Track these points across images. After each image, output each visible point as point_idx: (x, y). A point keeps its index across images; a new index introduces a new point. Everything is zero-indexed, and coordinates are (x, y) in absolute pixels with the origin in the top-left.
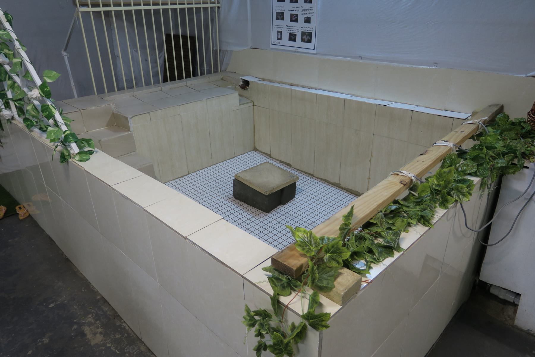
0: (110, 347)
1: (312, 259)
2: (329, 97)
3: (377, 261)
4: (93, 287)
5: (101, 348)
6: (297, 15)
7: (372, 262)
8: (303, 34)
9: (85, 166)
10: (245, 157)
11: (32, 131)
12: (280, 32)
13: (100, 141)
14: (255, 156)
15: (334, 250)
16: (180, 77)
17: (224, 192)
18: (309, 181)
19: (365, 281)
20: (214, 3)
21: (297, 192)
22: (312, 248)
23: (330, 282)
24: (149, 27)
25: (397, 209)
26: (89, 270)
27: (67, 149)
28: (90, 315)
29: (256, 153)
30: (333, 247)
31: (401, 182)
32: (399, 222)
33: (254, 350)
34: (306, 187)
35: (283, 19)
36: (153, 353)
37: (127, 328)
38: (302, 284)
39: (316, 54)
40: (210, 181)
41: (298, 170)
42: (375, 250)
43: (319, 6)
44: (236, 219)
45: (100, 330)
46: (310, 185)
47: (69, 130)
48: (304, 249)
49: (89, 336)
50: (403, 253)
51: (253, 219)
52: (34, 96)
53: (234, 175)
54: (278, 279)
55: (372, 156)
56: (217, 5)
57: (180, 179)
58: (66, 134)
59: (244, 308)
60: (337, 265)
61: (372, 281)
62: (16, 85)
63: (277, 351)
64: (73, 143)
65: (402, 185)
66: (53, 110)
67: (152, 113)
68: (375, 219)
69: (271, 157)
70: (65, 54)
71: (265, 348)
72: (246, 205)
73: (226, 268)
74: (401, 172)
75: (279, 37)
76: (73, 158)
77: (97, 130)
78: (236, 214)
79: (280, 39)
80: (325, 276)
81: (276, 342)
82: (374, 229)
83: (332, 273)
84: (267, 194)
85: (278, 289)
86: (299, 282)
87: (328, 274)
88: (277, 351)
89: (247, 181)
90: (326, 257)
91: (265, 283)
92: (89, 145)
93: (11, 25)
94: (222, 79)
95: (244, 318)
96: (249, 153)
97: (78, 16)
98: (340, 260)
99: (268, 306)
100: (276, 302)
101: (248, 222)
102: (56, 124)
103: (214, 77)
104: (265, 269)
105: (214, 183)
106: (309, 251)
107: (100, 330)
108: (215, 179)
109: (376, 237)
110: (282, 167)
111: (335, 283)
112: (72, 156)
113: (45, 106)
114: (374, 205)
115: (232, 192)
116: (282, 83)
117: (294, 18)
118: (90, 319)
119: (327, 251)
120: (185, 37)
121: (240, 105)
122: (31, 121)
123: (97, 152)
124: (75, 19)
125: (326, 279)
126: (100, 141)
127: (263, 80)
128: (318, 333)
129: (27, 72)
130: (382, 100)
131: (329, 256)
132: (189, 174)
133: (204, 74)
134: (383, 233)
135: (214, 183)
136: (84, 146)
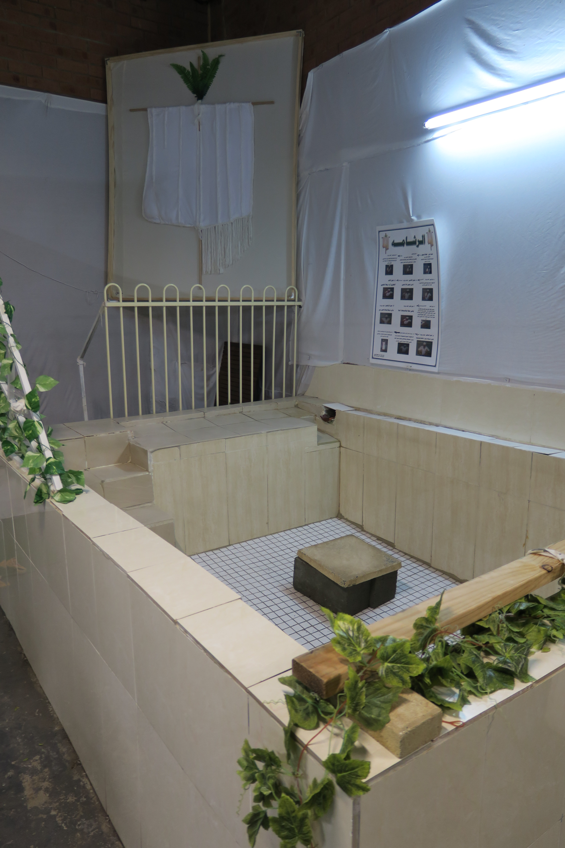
0: (55, 816)
1: (359, 669)
2: (456, 438)
3: (480, 692)
4: (53, 710)
5: (40, 816)
6: (411, 317)
7: (470, 693)
8: (419, 343)
9: (66, 509)
10: (322, 527)
11: (10, 459)
12: (385, 341)
13: (103, 482)
14: (338, 527)
15: (398, 656)
16: (235, 401)
17: (279, 578)
18: (421, 574)
19: (452, 723)
20: (294, 300)
21: (398, 590)
22: (358, 649)
23: (384, 711)
24: (211, 334)
25: (528, 609)
26: (50, 682)
27: (46, 484)
28: (37, 757)
29: (339, 522)
30: (394, 651)
31: (543, 567)
32: (533, 633)
33: (244, 821)
34: (416, 582)
35: (389, 322)
36: (119, 840)
37: (89, 787)
38: (336, 711)
39: (438, 373)
40: (261, 558)
41: (406, 554)
42: (478, 673)
43: (443, 305)
44: (292, 623)
45: (46, 784)
46: (422, 580)
47: (54, 458)
48: (344, 649)
49: (28, 792)
50: (531, 686)
51: (320, 627)
52: (18, 409)
53: (295, 549)
54: (301, 700)
55: (527, 537)
56: (297, 303)
57: (215, 552)
58: (49, 462)
59: (241, 745)
60: (400, 685)
61: (464, 724)
62: (3, 395)
63: (285, 833)
64: (56, 475)
65: (544, 572)
66: (39, 428)
67: (183, 448)
68: (487, 622)
69: (363, 530)
70: (80, 362)
71: (266, 823)
72: (311, 603)
73: (226, 674)
74: (545, 551)
75: (384, 348)
76: (52, 498)
77: (106, 467)
78: (292, 615)
79: (385, 351)
80: (376, 701)
81: (284, 814)
82: (484, 639)
83: (390, 696)
84: (346, 586)
85: (298, 718)
86: (332, 707)
87: (382, 699)
88: (285, 833)
89: (315, 561)
90: (382, 668)
91: (280, 704)
92: (78, 480)
93: (10, 318)
94: (297, 406)
95: (239, 762)
96: (329, 521)
97: (104, 312)
98: (407, 677)
99: (278, 747)
100: (292, 739)
101: (311, 630)
102: (39, 449)
103: (284, 403)
104: (283, 681)
105: (266, 562)
106: (354, 652)
107: (46, 784)
108: (268, 557)
109: (487, 654)
110: (379, 547)
111: (392, 716)
112: (52, 494)
113: (30, 422)
114: (487, 597)
115: (291, 580)
116: (385, 415)
117: (407, 322)
118: (36, 763)
119: (385, 658)
120: (247, 347)
121: (318, 444)
122: (12, 446)
123: (87, 492)
124: (100, 316)
125: (377, 706)
126: (103, 482)
127: (357, 409)
128: (350, 801)
129: (17, 377)
130: (544, 447)
131: (388, 668)
132: (230, 545)
133: (270, 398)
134: (498, 647)
135: (266, 562)
136: (72, 483)
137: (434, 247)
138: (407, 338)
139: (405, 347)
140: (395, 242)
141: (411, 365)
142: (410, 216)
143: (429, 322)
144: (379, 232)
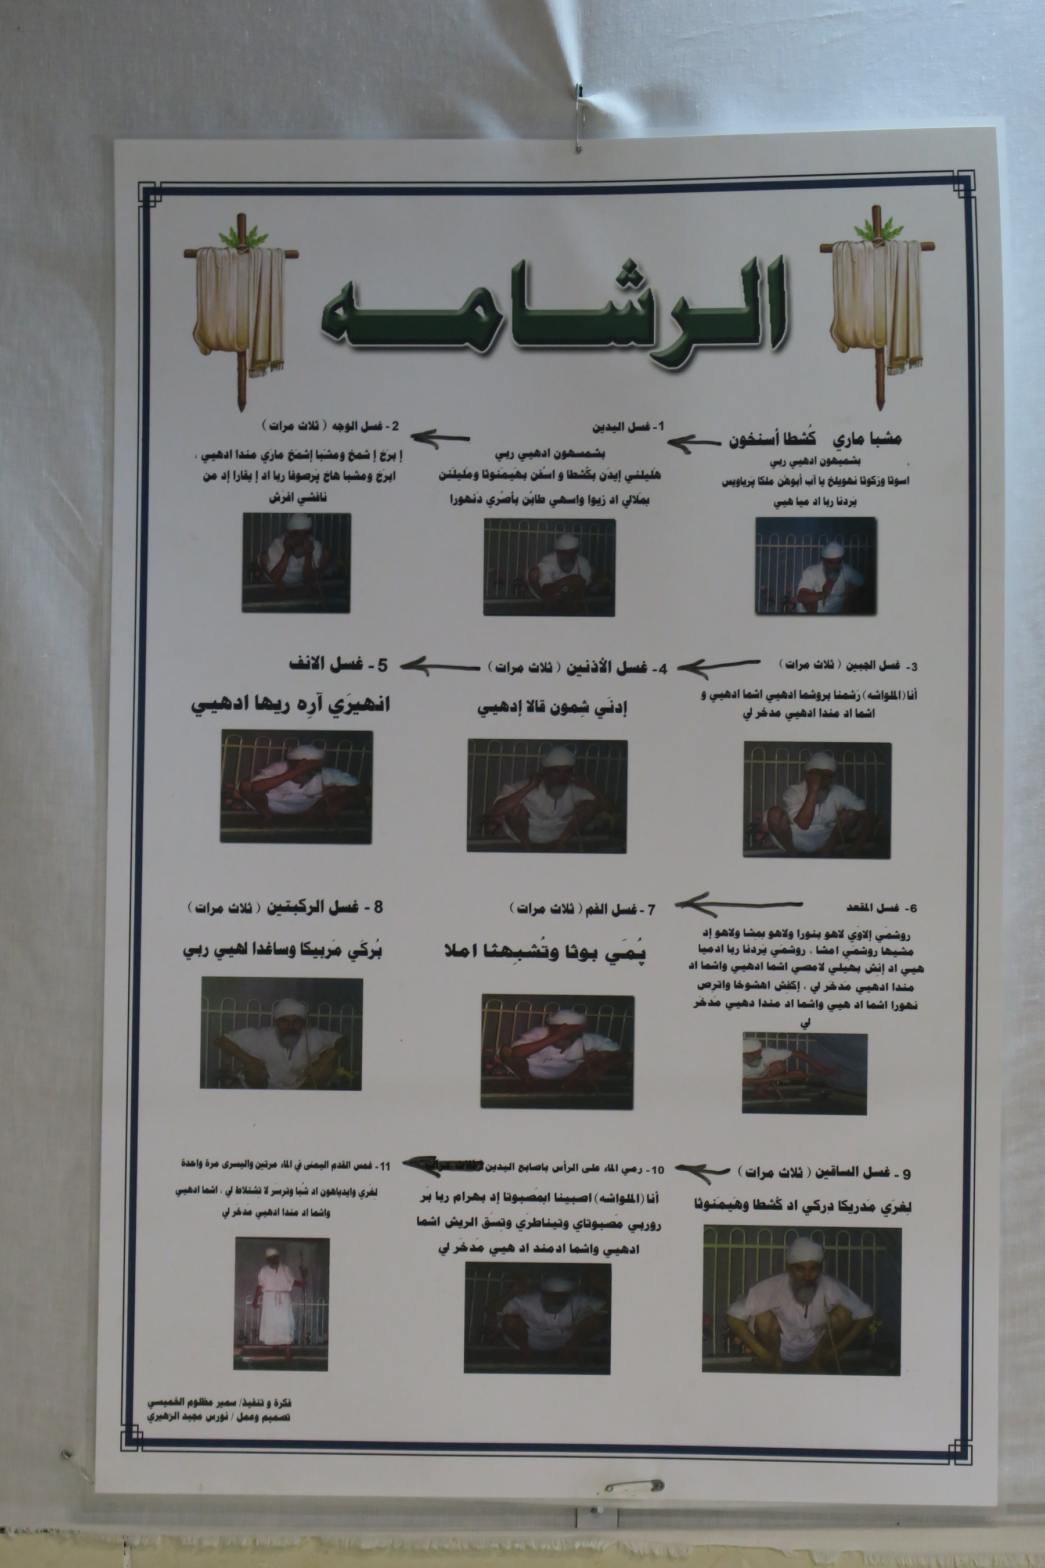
6: (614, 1015)
75: (277, 1325)
79: (308, 1352)
137: (925, 399)
138: (574, 1213)
139: (554, 1302)
140: (368, 302)
141: (648, 1467)
142: (953, 177)
143: (854, 1048)
144: (151, 194)
